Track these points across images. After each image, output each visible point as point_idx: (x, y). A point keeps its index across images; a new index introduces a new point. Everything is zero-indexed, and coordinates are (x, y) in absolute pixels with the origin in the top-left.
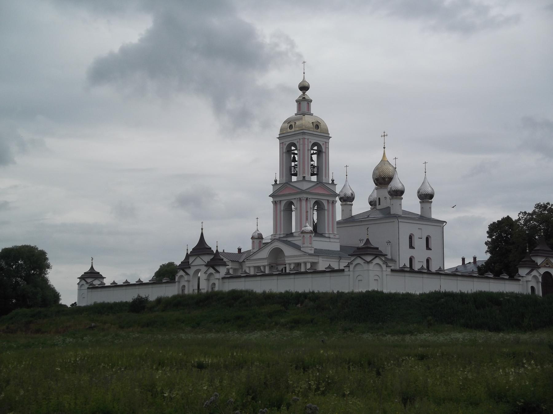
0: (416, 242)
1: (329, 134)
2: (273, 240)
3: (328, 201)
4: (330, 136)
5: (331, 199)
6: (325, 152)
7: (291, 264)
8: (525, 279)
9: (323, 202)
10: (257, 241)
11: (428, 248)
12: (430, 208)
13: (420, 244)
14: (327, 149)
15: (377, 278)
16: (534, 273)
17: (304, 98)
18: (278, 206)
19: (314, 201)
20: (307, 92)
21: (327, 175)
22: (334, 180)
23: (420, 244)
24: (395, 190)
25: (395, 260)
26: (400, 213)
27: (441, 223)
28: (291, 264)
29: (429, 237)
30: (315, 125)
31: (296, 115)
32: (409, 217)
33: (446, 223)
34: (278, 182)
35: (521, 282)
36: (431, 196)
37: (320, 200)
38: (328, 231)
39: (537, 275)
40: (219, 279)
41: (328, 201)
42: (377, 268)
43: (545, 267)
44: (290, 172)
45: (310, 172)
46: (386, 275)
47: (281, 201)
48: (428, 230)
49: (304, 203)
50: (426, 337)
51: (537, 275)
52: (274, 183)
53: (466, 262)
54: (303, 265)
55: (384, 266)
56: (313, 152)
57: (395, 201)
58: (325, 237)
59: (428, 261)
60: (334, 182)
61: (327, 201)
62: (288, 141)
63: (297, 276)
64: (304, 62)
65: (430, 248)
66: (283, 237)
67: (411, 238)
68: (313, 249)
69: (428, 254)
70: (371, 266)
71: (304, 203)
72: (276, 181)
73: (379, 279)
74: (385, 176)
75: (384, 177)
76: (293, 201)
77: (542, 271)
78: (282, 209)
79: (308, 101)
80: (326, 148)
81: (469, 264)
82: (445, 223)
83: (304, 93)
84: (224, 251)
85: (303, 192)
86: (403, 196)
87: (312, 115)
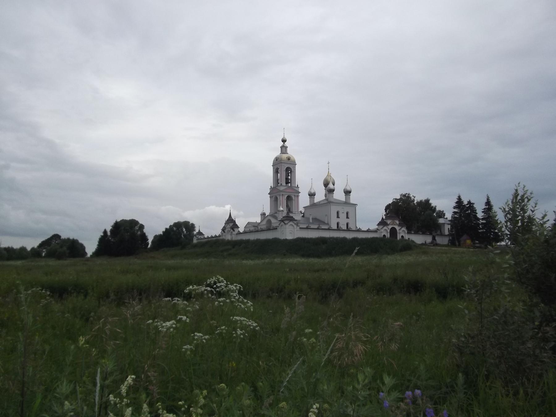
0: (341, 215)
3: (295, 195)
5: (296, 194)
6: (294, 172)
8: (380, 231)
10: (263, 216)
11: (347, 217)
12: (349, 198)
13: (343, 216)
14: (295, 170)
15: (291, 232)
16: (385, 228)
17: (284, 146)
18: (272, 199)
21: (295, 183)
23: (343, 216)
26: (332, 200)
27: (355, 205)
30: (287, 158)
31: (280, 154)
32: (339, 203)
34: (272, 187)
35: (378, 233)
36: (350, 192)
38: (295, 210)
39: (387, 229)
40: (235, 234)
42: (291, 227)
43: (392, 224)
46: (297, 230)
48: (347, 209)
49: (281, 197)
50: (233, 262)
51: (387, 229)
52: (270, 188)
55: (295, 226)
57: (331, 195)
58: (293, 213)
61: (294, 196)
62: (276, 167)
63: (261, 232)
64: (347, 176)
66: (274, 214)
67: (338, 213)
69: (348, 220)
70: (287, 226)
71: (281, 197)
72: (271, 187)
73: (292, 232)
77: (390, 227)
78: (273, 200)
80: (294, 169)
83: (284, 143)
85: (281, 191)
86: (334, 192)
87: (288, 154)
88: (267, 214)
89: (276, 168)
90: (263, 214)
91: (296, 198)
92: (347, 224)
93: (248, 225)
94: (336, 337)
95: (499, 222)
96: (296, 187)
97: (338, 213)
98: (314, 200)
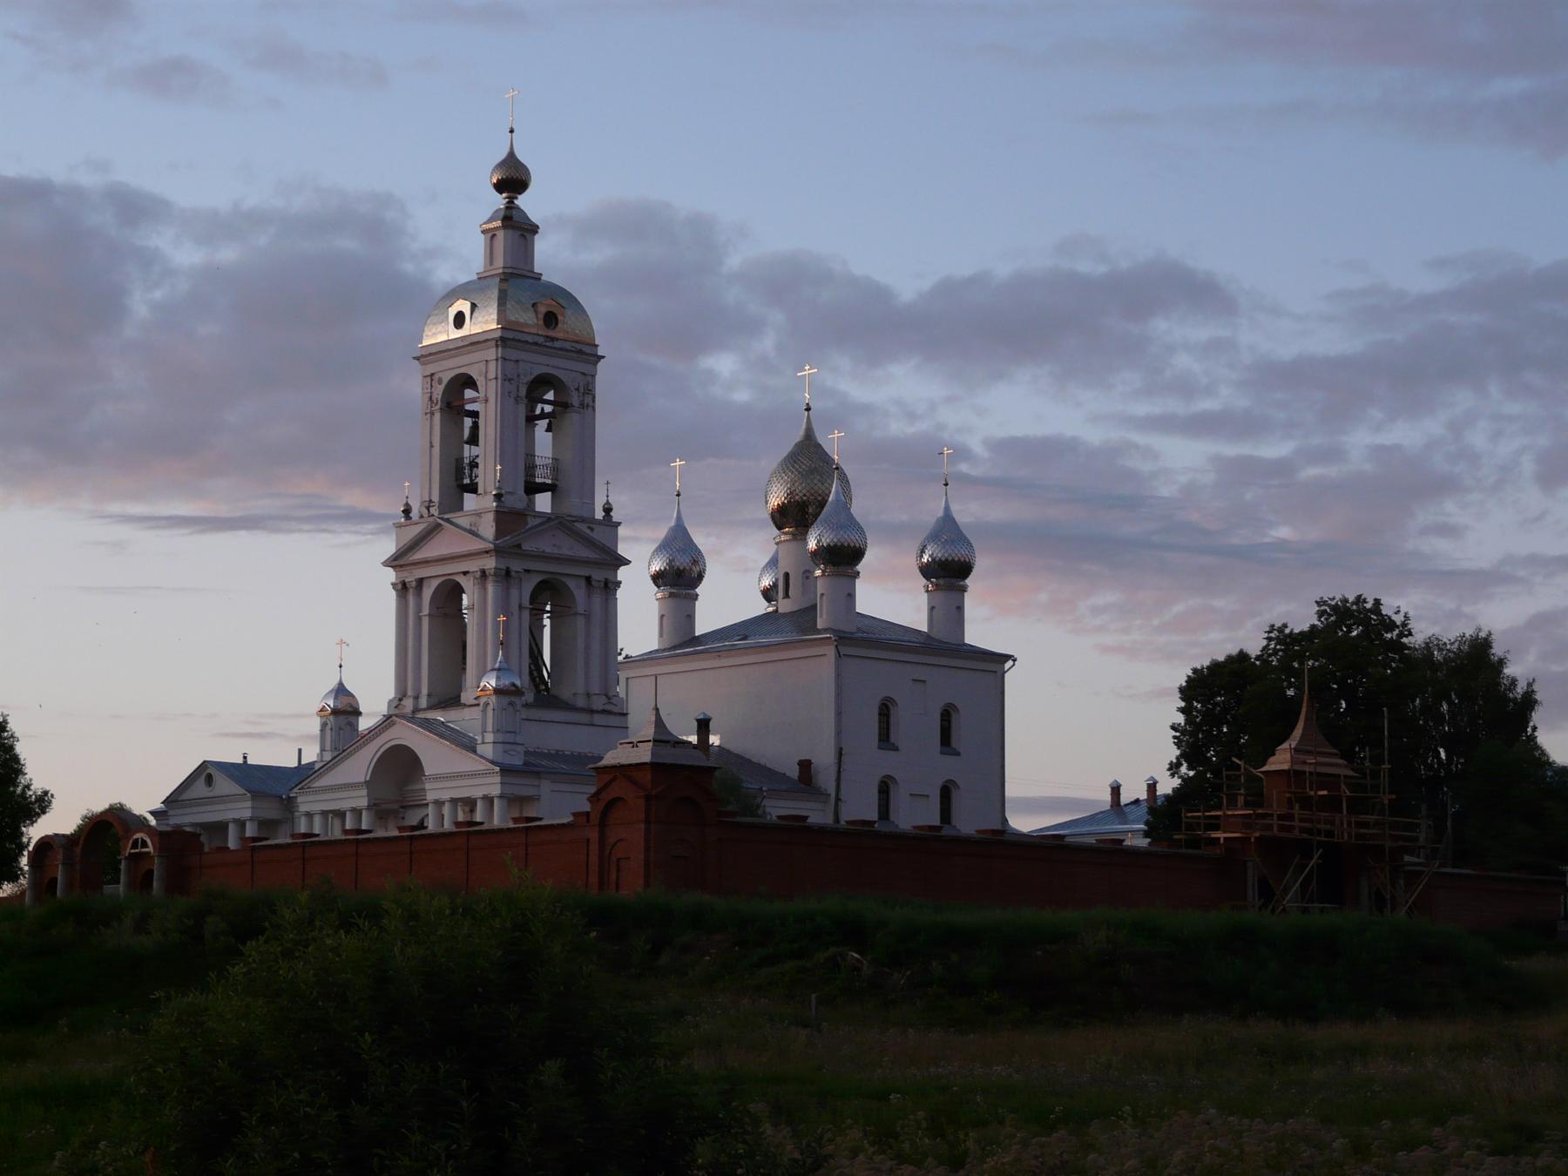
1: (597, 346)
2: (388, 721)
4: (599, 354)
5: (598, 575)
7: (443, 803)
9: (567, 583)
18: (411, 598)
19: (536, 579)
20: (519, 197)
22: (611, 510)
24: (832, 544)
25: (825, 790)
27: (995, 663)
28: (443, 803)
29: (950, 710)
33: (1015, 660)
37: (558, 577)
41: (588, 579)
44: (457, 480)
45: (480, 471)
47: (420, 582)
53: (1125, 798)
54: (232, 830)
56: (543, 409)
59: (946, 792)
60: (611, 514)
61: (583, 582)
65: (955, 749)
67: (885, 710)
68: (521, 749)
74: (805, 495)
75: (804, 502)
76: (461, 580)
79: (524, 229)
81: (1133, 807)
82: (1010, 663)
84: (245, 758)
88: (375, 700)
89: (447, 377)
90: (343, 711)
91: (597, 600)
92: (946, 792)
93: (200, 789)
94: (1293, 823)
95: (8, 729)
96: (593, 520)
97: (885, 710)
98: (690, 618)
